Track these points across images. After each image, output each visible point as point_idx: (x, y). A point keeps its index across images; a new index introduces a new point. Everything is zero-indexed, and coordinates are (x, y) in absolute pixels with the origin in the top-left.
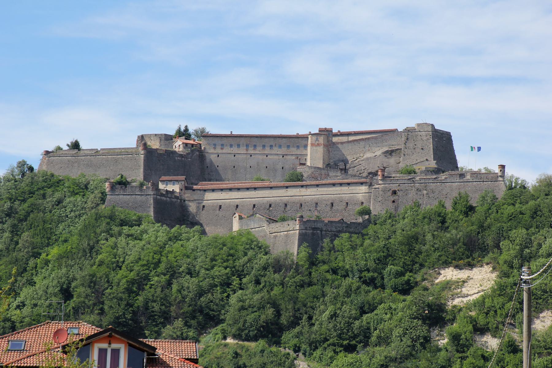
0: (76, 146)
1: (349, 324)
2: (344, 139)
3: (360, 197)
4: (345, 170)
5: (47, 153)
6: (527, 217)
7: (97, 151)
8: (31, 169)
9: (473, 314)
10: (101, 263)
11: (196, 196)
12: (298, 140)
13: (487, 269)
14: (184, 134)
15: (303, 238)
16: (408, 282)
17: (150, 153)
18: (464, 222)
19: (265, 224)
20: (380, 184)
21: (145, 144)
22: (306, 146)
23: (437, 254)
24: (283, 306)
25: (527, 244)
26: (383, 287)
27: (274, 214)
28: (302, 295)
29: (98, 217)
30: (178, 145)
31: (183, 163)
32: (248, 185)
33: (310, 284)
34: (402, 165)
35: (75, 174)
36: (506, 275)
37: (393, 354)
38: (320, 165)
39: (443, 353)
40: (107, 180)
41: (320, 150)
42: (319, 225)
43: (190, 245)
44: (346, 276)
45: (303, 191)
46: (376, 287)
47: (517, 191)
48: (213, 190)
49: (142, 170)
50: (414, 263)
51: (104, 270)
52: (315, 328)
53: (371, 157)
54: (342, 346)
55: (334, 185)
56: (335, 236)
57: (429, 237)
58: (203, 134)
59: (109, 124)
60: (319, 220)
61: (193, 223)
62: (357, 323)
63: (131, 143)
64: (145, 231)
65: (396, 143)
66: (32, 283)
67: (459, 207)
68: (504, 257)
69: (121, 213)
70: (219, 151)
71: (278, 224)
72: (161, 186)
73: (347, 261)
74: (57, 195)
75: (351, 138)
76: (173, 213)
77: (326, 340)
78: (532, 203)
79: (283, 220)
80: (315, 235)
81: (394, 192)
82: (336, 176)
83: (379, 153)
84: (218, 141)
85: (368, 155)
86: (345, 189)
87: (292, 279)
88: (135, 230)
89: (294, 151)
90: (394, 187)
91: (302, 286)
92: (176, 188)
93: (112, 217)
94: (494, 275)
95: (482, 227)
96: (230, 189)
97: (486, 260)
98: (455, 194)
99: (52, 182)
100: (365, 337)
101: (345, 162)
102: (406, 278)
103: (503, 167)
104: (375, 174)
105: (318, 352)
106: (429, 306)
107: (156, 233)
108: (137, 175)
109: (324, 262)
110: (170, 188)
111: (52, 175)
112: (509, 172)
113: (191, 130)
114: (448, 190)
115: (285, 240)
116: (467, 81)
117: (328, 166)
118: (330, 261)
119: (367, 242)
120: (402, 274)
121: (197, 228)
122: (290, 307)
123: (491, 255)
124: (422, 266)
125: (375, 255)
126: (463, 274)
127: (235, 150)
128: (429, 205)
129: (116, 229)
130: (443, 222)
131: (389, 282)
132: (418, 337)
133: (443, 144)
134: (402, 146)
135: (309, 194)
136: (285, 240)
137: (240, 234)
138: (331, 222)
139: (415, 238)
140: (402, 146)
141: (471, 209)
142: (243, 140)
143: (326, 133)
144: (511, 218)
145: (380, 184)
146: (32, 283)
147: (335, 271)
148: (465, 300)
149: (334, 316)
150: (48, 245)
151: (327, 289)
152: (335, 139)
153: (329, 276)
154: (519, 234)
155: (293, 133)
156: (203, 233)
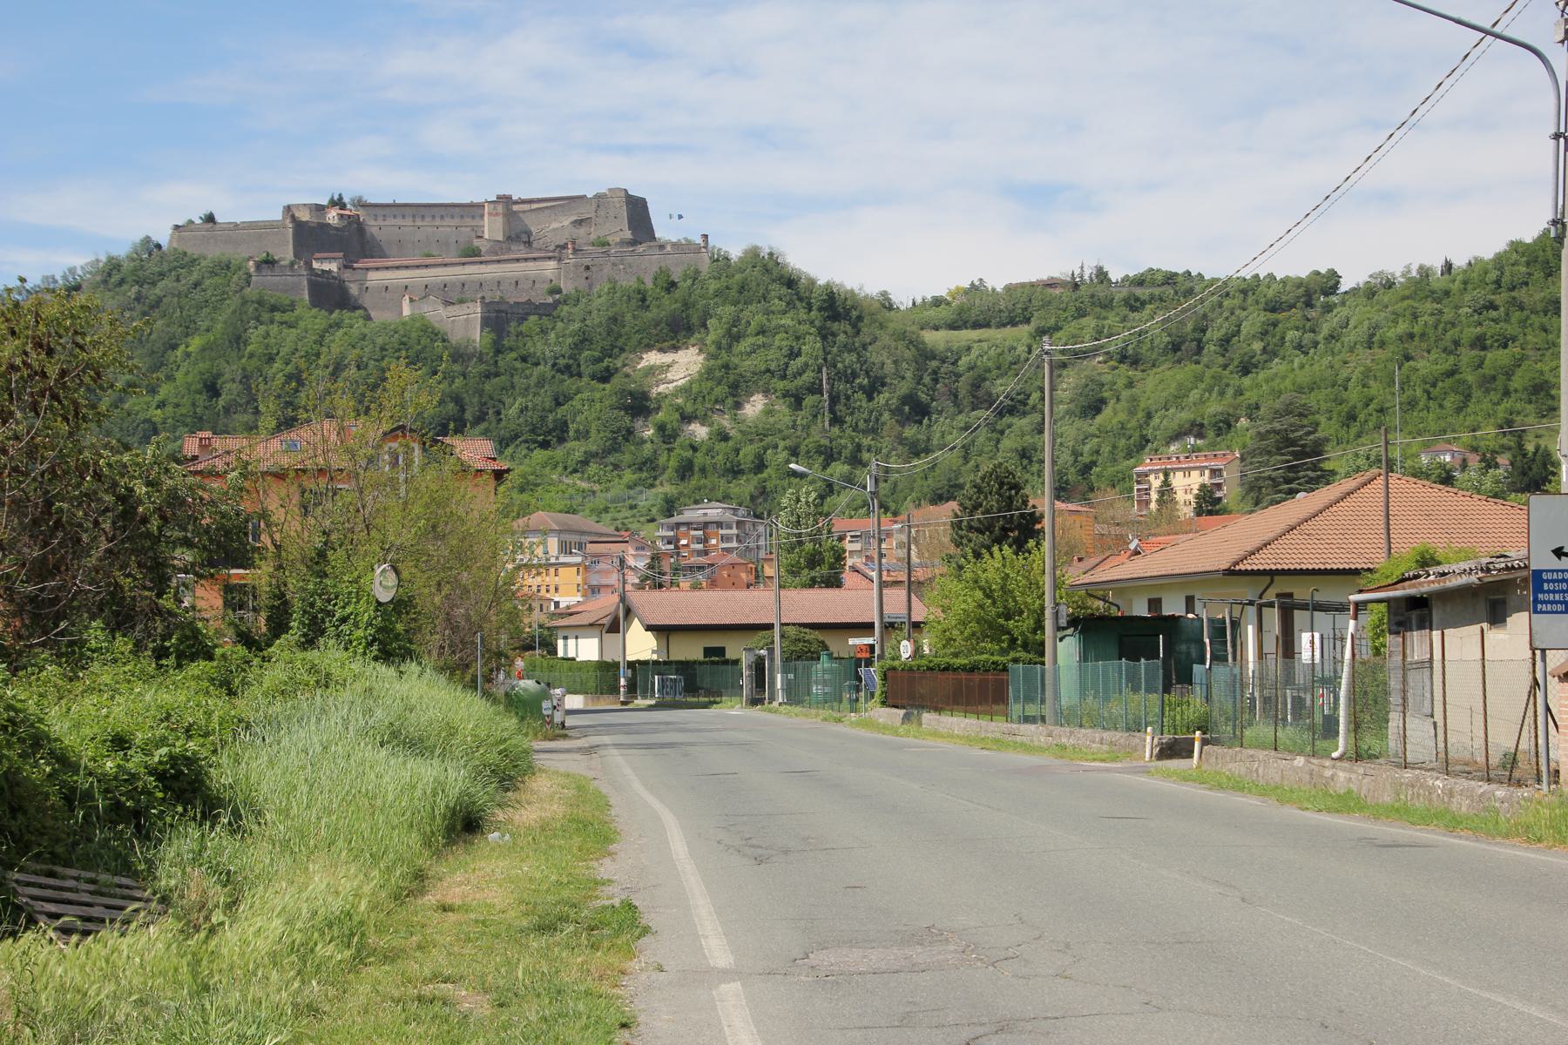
0: (210, 219)
1: (543, 418)
2: (526, 207)
3: (549, 274)
4: (529, 243)
5: (177, 227)
6: (733, 293)
7: (236, 225)
8: (159, 246)
9: (679, 401)
10: (251, 356)
11: (358, 275)
12: (473, 209)
13: (693, 351)
14: (338, 203)
15: (486, 322)
16: (607, 369)
17: (299, 226)
18: (666, 300)
19: (441, 307)
20: (570, 259)
21: (293, 216)
22: (482, 216)
23: (638, 336)
24: (467, 400)
25: (736, 322)
26: (580, 375)
27: (451, 295)
28: (487, 387)
29: (245, 302)
30: (332, 216)
31: (338, 239)
32: (417, 262)
33: (497, 375)
34: (593, 237)
35: (214, 252)
36: (714, 357)
37: (594, 448)
38: (500, 238)
39: (648, 445)
40: (251, 258)
41: (500, 220)
42: (503, 307)
43: (355, 332)
44: (537, 364)
45: (483, 269)
46: (571, 376)
47: (721, 262)
48: (377, 269)
49: (291, 246)
50: (613, 347)
51: (255, 362)
52: (503, 423)
53: (557, 227)
54: (535, 442)
55: (518, 260)
56: (524, 319)
57: (628, 317)
58: (361, 204)
59: (252, 193)
60: (502, 301)
61: (355, 308)
62: (551, 417)
63: (277, 215)
64: (299, 318)
65: (586, 211)
66: (170, 378)
67: (659, 282)
68: (710, 339)
69: (272, 297)
70: (380, 222)
71: (456, 307)
72: (316, 265)
73: (537, 347)
74: (195, 276)
75: (535, 206)
76: (331, 295)
77: (517, 436)
78: (738, 277)
79: (461, 302)
80: (499, 318)
81: (587, 268)
82: (519, 251)
83: (566, 223)
84: (380, 212)
85: (555, 225)
86: (531, 264)
87: (474, 369)
88: (286, 317)
89: (469, 221)
90: (587, 261)
91: (488, 377)
92: (333, 267)
93: (260, 303)
94: (701, 358)
95: (686, 305)
96: (398, 268)
97: (692, 340)
98: (656, 269)
99: (180, 262)
100: (561, 432)
101: (529, 234)
102: (605, 364)
103: (706, 236)
104: (565, 247)
105: (510, 450)
106: (631, 394)
107: (314, 320)
108: (286, 253)
109: (512, 350)
110: (326, 266)
111: (185, 254)
112: (711, 242)
113: (346, 200)
114: (644, 267)
115: (465, 325)
116: (627, 150)
117: (509, 239)
118: (518, 348)
119: (560, 325)
120: (600, 360)
121: (359, 312)
122: (475, 400)
123: (697, 335)
124: (622, 350)
125: (570, 340)
126: (667, 358)
127: (399, 221)
128: (628, 282)
129: (266, 316)
130: (643, 300)
131: (587, 369)
132: (619, 430)
133: (637, 211)
134: (592, 215)
135: (490, 271)
136: (465, 325)
137: (413, 318)
138: (517, 303)
139: (614, 319)
140: (592, 215)
141: (673, 284)
142: (408, 211)
143: (505, 200)
144: (717, 294)
145: (570, 259)
146: (170, 378)
147: (524, 359)
148: (671, 386)
149: (523, 410)
150: (187, 335)
151: (516, 379)
152: (515, 208)
153: (518, 365)
154: (727, 311)
155: (466, 199)
156: (368, 318)
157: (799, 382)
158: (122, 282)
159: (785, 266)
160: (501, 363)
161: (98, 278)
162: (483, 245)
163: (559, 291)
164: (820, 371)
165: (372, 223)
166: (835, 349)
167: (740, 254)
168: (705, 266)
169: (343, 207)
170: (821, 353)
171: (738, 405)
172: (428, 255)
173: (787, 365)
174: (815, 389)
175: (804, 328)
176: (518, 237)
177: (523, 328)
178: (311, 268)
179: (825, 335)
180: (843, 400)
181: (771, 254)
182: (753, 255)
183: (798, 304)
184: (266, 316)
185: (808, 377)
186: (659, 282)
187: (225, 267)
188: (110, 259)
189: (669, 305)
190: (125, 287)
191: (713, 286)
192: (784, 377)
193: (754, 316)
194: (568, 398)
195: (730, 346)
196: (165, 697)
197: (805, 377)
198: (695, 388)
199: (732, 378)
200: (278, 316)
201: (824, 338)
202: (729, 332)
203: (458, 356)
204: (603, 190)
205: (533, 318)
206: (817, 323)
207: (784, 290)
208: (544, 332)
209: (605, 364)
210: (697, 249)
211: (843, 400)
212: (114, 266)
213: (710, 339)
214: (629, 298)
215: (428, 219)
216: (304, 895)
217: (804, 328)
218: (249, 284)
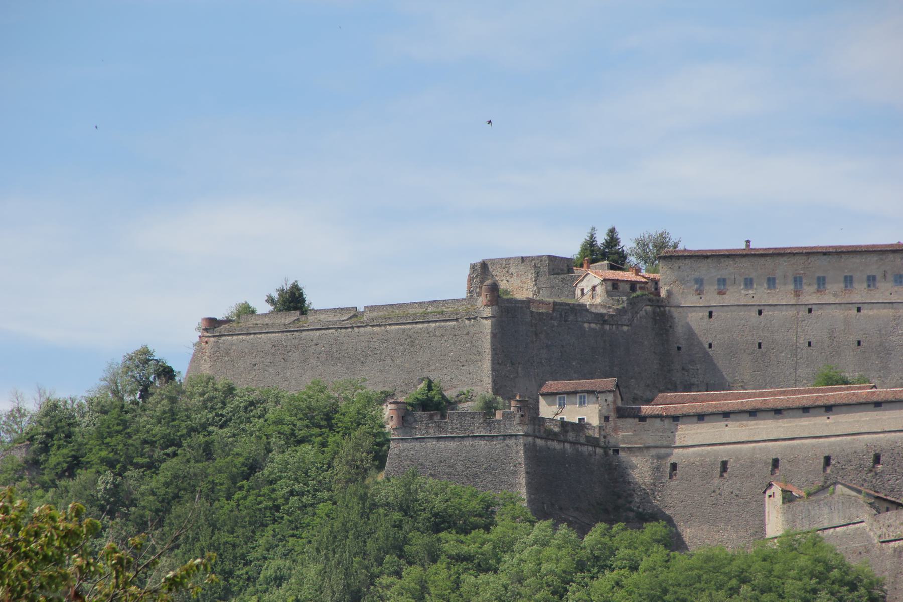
0: (292, 300)
5: (212, 324)
7: (355, 314)
8: (167, 373)
11: (651, 435)
17: (508, 312)
19: (866, 514)
21: (494, 289)
30: (591, 288)
32: (805, 399)
40: (387, 396)
48: (701, 417)
49: (487, 364)
58: (663, 253)
61: (643, 517)
63: (452, 285)
69: (434, 493)
72: (547, 410)
76: (584, 487)
88: (471, 545)
92: (590, 414)
96: (753, 413)
108: (472, 379)
110: (572, 413)
113: (627, 243)
121: (653, 529)
127: (760, 295)
137: (790, 543)
142: (783, 267)
156: (675, 542)
158: (74, 465)
161: (19, 456)
165: (691, 300)
169: (618, 261)
172: (832, 381)
178: (536, 420)
184: (418, 542)
187: (324, 420)
188: (52, 409)
190: (83, 475)
200: (450, 541)
212: (56, 426)
215: (835, 288)
218: (380, 460)
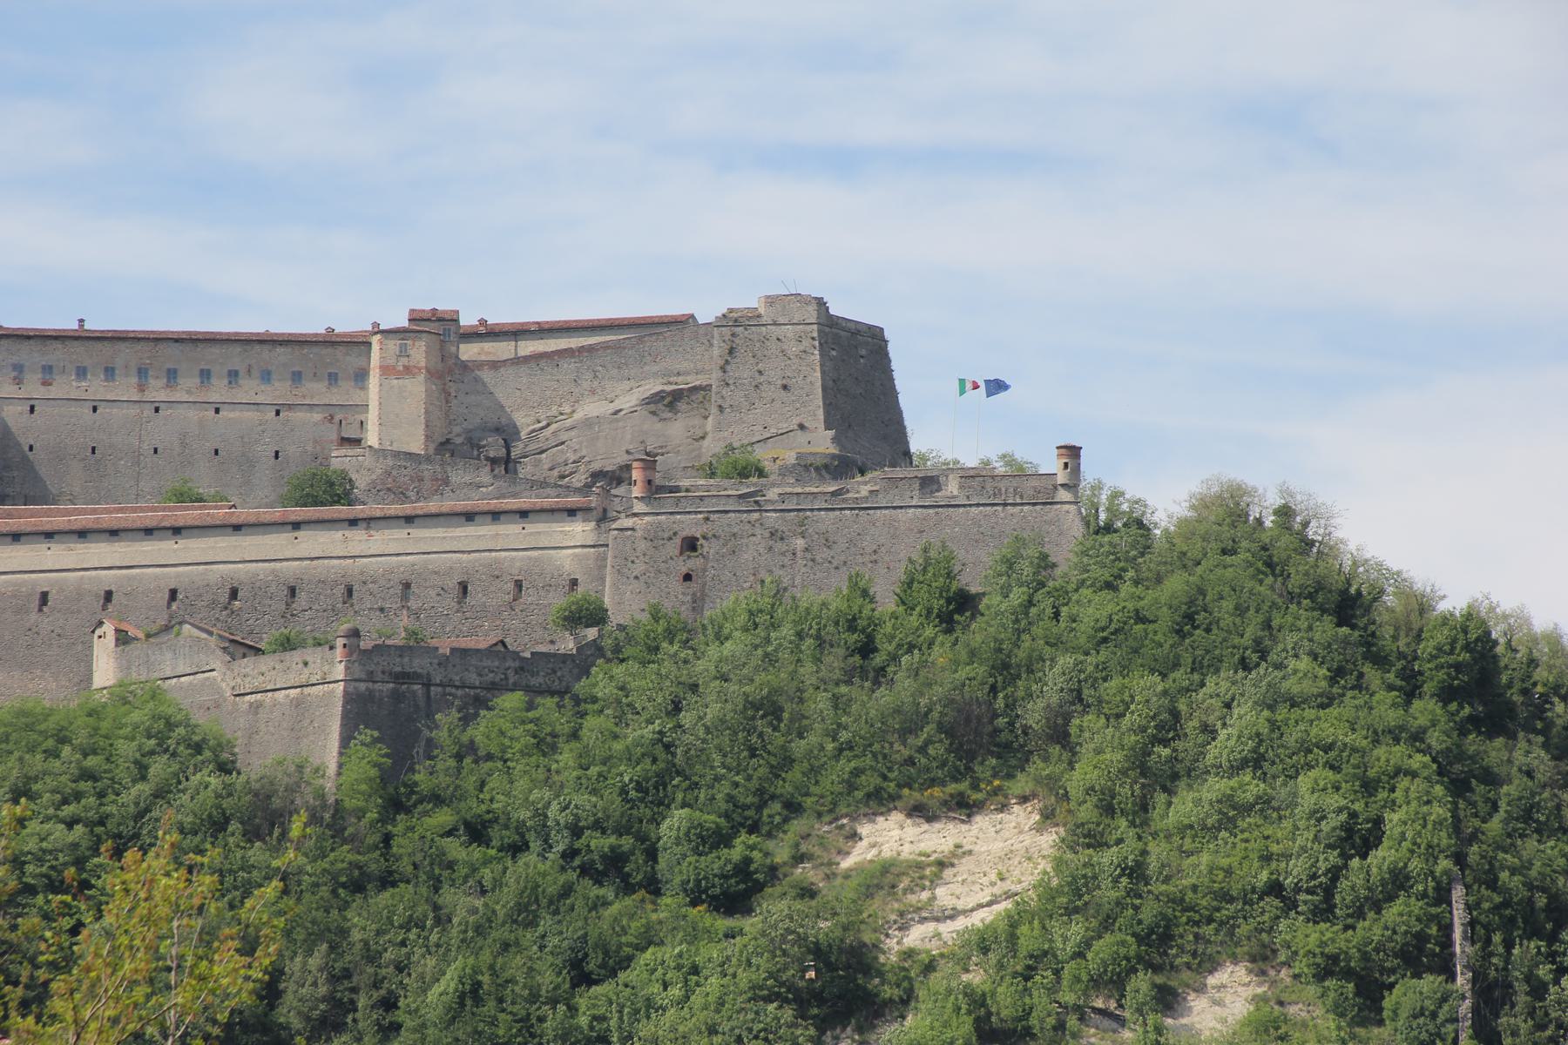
2: (503, 350)
3: (566, 562)
4: (506, 464)
6: (1161, 630)
9: (975, 978)
12: (332, 354)
13: (1022, 817)
15: (358, 711)
16: (743, 869)
19: (217, 661)
20: (637, 515)
22: (361, 376)
23: (845, 766)
25: (1168, 727)
26: (654, 887)
27: (246, 624)
33: (387, 881)
34: (711, 447)
38: (417, 445)
41: (416, 390)
42: (418, 664)
45: (359, 541)
46: (628, 888)
47: (1122, 536)
53: (598, 416)
55: (469, 517)
56: (477, 703)
57: (820, 703)
60: (415, 645)
67: (921, 594)
68: (1083, 775)
71: (265, 663)
73: (516, 793)
75: (528, 347)
78: (1177, 584)
79: (287, 644)
80: (400, 700)
81: (691, 545)
82: (475, 485)
83: (628, 401)
84: (31, 356)
85: (592, 408)
86: (510, 531)
89: (317, 391)
90: (689, 525)
91: (357, 887)
94: (1048, 840)
95: (1005, 670)
96: (82, 534)
97: (1022, 784)
101: (508, 433)
102: (736, 852)
103: (1072, 453)
104: (618, 477)
109: (437, 799)
112: (1090, 470)
114: (876, 547)
115: (294, 719)
116: (842, 162)
120: (721, 839)
123: (1037, 766)
124: (793, 808)
126: (936, 838)
127: (96, 387)
128: (822, 591)
130: (867, 649)
131: (678, 864)
133: (856, 367)
134: (713, 378)
136: (294, 719)
137: (123, 696)
139: (769, 708)
140: (713, 378)
141: (964, 603)
142: (125, 352)
143: (436, 327)
145: (637, 515)
147: (476, 832)
148: (948, 929)
151: (447, 896)
152: (469, 351)
153: (455, 849)
155: (311, 325)
157: (1372, 929)
159: (1328, 551)
160: (401, 846)
162: (358, 468)
163: (596, 616)
164: (1442, 896)
166: (1495, 826)
167: (1182, 510)
168: (1065, 536)
170: (1444, 839)
171: (1167, 1000)
172: (184, 497)
173: (1335, 874)
174: (1424, 953)
175: (1387, 755)
176: (476, 444)
177: (478, 732)
179: (1462, 779)
180: (1522, 999)
181: (1285, 513)
182: (1226, 517)
183: (1372, 675)
185: (1400, 913)
186: (921, 594)
189: (946, 670)
191: (1094, 609)
192: (1323, 912)
193: (1232, 714)
194: (616, 963)
195: (1144, 806)
196: (884, 697)
197: (1392, 912)
198: (1029, 939)
199: (1149, 912)
201: (1459, 787)
202: (1139, 763)
203: (264, 817)
204: (749, 300)
205: (511, 701)
206: (1435, 739)
207: (1326, 629)
208: (545, 745)
209: (736, 852)
210: (1042, 493)
211: (1522, 999)
213: (1083, 775)
214: (821, 642)
215: (188, 382)
216: (609, 654)
217: (1387, 755)
